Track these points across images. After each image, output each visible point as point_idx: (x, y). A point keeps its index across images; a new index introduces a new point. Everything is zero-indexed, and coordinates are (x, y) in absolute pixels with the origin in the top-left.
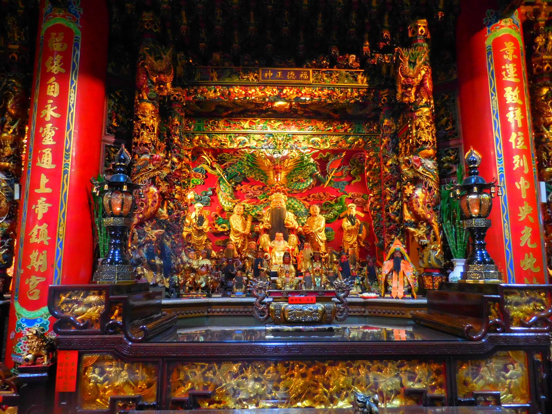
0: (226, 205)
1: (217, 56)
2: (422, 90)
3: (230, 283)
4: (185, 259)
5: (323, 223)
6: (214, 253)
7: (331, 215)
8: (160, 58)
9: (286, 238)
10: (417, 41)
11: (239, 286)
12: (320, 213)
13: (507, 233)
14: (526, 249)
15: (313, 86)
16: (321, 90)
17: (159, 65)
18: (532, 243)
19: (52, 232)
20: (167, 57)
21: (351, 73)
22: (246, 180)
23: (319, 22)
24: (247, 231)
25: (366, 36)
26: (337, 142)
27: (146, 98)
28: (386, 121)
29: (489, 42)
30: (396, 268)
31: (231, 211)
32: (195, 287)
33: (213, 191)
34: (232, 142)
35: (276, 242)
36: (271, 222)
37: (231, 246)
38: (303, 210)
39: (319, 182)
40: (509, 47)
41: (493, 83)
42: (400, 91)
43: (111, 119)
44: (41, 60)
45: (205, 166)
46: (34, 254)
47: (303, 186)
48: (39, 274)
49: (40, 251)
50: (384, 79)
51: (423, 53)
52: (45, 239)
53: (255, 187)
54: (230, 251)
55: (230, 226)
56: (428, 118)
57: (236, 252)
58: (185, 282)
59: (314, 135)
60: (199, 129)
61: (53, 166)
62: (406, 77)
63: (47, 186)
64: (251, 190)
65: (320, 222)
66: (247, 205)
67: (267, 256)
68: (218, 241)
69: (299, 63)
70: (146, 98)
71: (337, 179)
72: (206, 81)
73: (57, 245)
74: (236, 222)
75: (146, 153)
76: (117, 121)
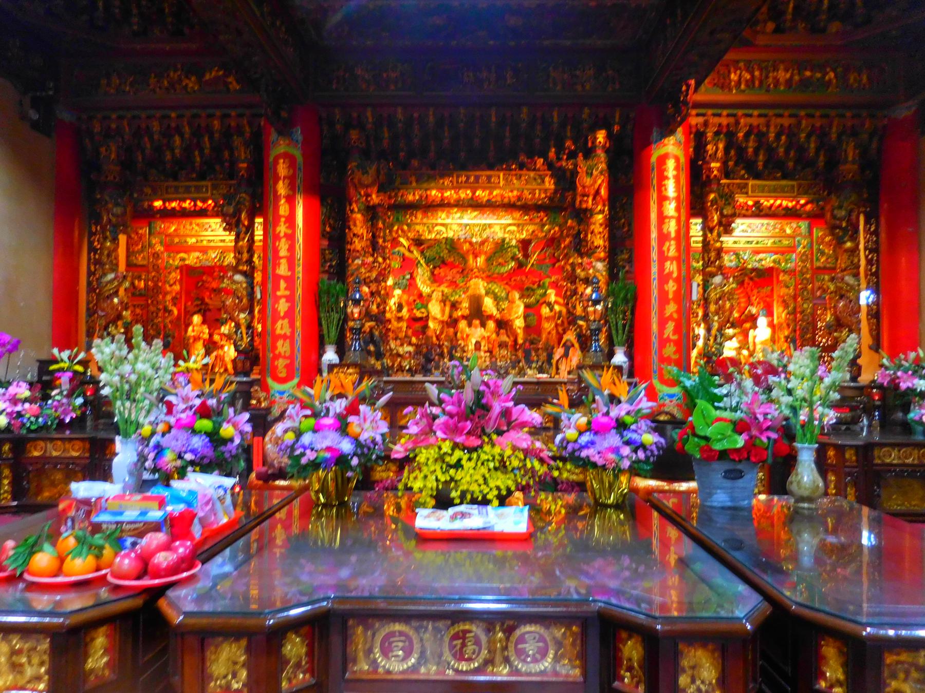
0: (425, 290)
1: (415, 163)
2: (598, 198)
3: (429, 366)
4: (393, 346)
5: (521, 309)
6: (414, 340)
7: (532, 299)
8: (367, 172)
9: (483, 325)
10: (595, 151)
11: (437, 368)
12: (520, 298)
13: (655, 327)
14: (668, 340)
15: (503, 185)
16: (512, 191)
17: (367, 179)
18: (674, 334)
19: (292, 325)
20: (372, 170)
21: (540, 176)
22: (444, 263)
23: (507, 134)
24: (446, 318)
25: (552, 143)
26: (533, 232)
27: (356, 210)
28: (570, 221)
29: (654, 159)
30: (566, 355)
31: (430, 296)
32: (401, 369)
33: (412, 274)
34: (430, 232)
35: (473, 329)
36: (470, 308)
37: (430, 333)
38: (504, 294)
39: (520, 265)
40: (671, 164)
41: (654, 196)
42: (578, 199)
43: (324, 225)
44: (271, 182)
45: (402, 249)
46: (280, 343)
47: (504, 270)
48: (285, 357)
49: (285, 340)
50: (566, 181)
51: (601, 163)
52: (287, 331)
53: (455, 271)
54: (428, 338)
55: (428, 313)
56: (601, 225)
57: (434, 339)
58: (393, 365)
59: (510, 225)
60: (398, 219)
61: (289, 274)
62: (584, 187)
63: (286, 289)
64: (450, 274)
65: (520, 308)
66: (446, 290)
67: (698, 262)
68: (418, 326)
69: (491, 167)
70: (356, 210)
71: (540, 261)
72: (406, 183)
73: (296, 335)
74: (435, 309)
75: (358, 258)
76: (330, 226)
